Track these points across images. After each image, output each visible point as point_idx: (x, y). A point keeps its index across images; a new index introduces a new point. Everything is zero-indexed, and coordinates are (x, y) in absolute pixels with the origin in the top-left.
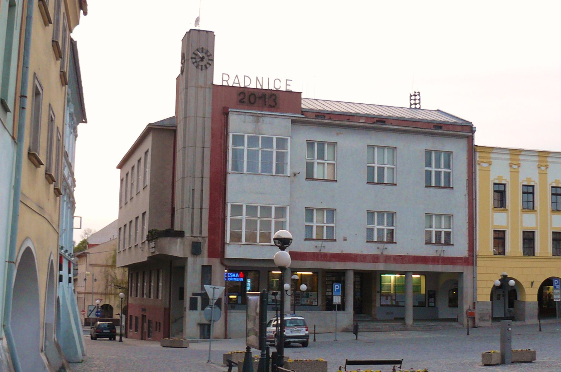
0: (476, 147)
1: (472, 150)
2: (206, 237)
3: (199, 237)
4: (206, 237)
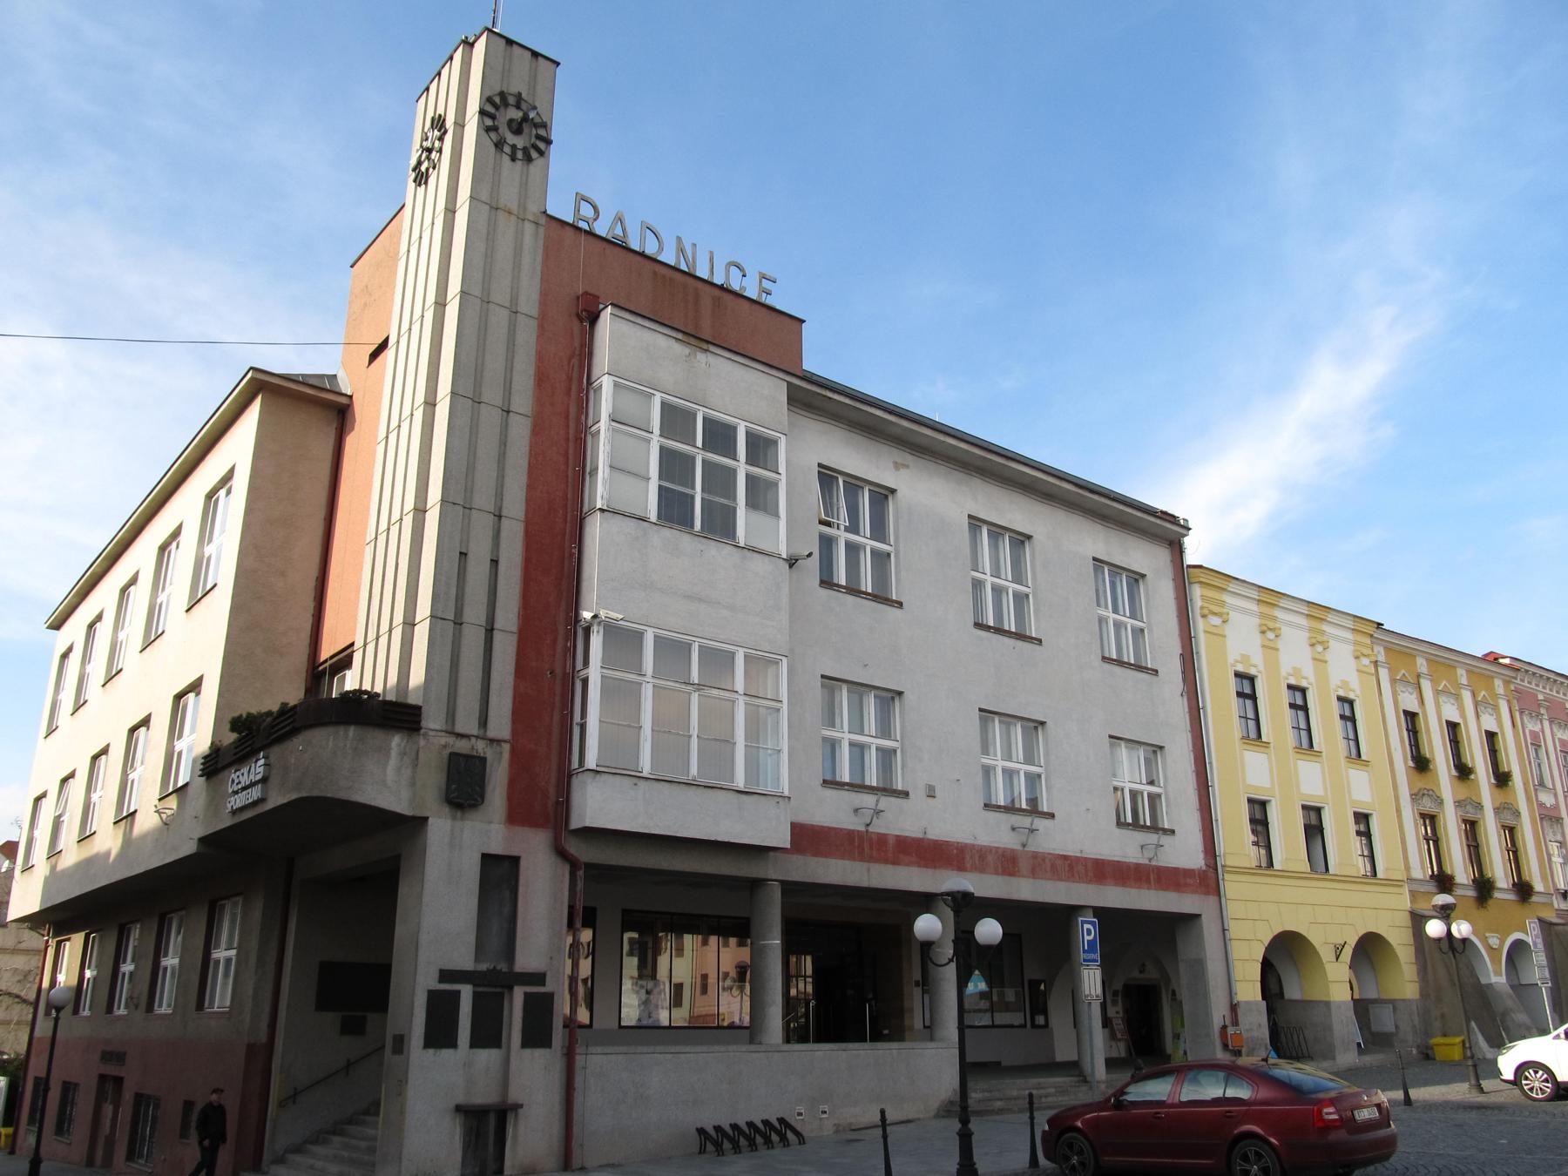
0: (1191, 570)
1: (1183, 575)
2: (505, 741)
3: (477, 737)
4: (505, 741)
